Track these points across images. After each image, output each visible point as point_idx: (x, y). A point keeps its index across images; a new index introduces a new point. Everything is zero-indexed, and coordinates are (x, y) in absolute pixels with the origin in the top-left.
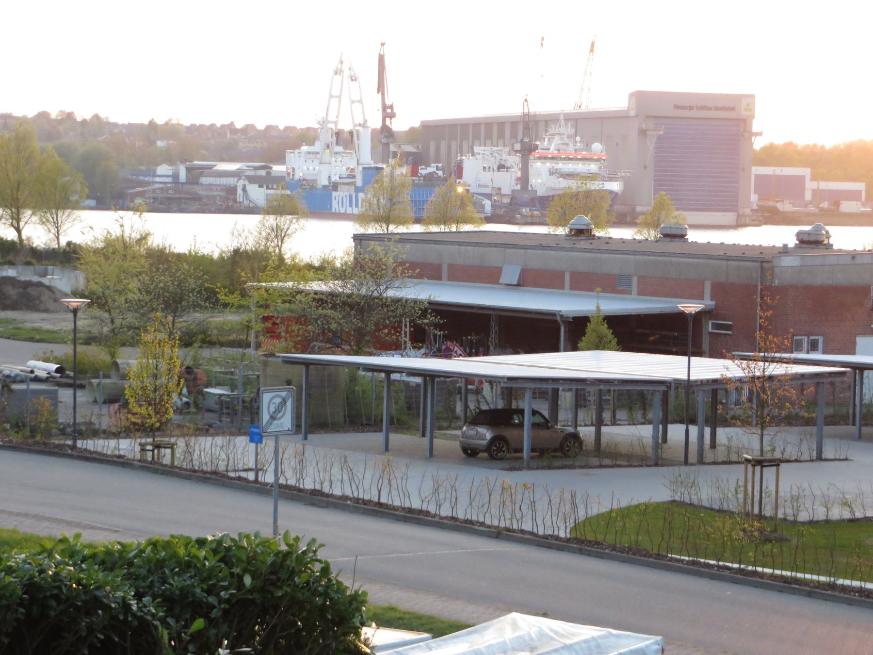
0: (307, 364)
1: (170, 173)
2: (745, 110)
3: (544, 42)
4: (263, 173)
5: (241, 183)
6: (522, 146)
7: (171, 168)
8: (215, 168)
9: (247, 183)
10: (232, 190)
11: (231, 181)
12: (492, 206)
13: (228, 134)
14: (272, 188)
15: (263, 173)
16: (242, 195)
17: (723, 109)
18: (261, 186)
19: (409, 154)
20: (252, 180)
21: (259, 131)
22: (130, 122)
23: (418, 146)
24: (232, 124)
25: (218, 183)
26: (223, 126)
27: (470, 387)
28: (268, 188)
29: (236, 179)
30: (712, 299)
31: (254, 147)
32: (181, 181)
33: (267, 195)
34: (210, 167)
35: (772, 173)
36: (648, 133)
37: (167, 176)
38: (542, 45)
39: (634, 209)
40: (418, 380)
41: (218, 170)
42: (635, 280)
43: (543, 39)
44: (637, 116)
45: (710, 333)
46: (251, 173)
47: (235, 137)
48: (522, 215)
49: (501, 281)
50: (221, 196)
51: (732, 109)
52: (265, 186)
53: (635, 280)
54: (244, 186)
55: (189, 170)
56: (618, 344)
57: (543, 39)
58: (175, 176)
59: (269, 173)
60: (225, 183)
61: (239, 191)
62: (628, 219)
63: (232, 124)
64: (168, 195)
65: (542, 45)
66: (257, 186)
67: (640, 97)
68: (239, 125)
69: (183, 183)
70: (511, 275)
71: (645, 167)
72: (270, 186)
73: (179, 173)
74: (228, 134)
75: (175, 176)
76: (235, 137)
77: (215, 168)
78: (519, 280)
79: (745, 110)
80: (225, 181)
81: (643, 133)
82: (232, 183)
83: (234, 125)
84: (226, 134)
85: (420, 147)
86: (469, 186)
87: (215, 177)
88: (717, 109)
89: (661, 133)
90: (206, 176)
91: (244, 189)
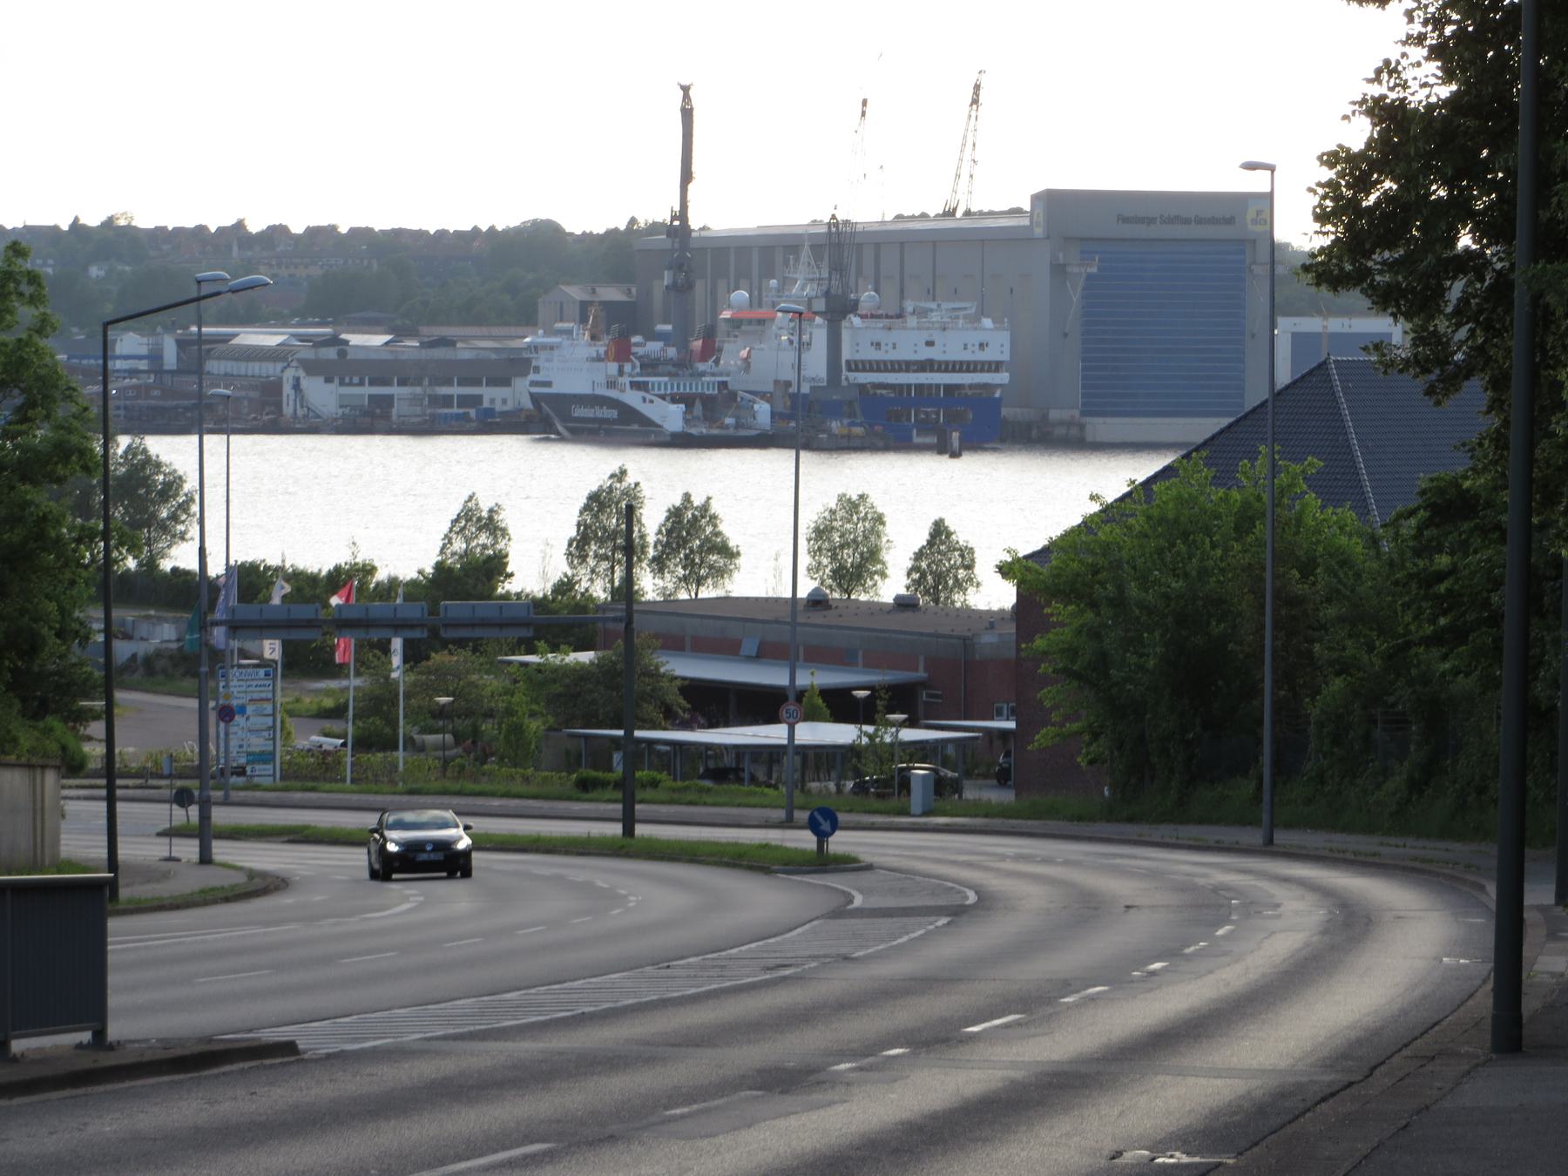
0: (586, 737)
1: (144, 351)
2: (1254, 222)
3: (868, 110)
4: (331, 353)
5: (289, 374)
6: (827, 304)
7: (145, 340)
8: (235, 341)
9: (301, 373)
10: (272, 389)
11: (270, 369)
12: (773, 414)
13: (235, 249)
14: (351, 384)
15: (331, 353)
16: (292, 397)
17: (1213, 221)
18: (329, 380)
19: (608, 306)
20: (312, 368)
21: (297, 237)
22: (30, 223)
23: (629, 290)
24: (240, 225)
25: (243, 372)
26: (221, 230)
27: (709, 752)
28: (342, 383)
29: (279, 366)
30: (925, 671)
31: (291, 276)
32: (166, 367)
33: (341, 396)
34: (226, 339)
35: (1320, 330)
36: (1069, 269)
37: (140, 358)
38: (863, 114)
39: (1045, 417)
40: (668, 748)
41: (240, 346)
42: (860, 653)
43: (865, 103)
44: (1048, 238)
45: (926, 703)
46: (308, 354)
47: (249, 253)
48: (831, 435)
49: (741, 653)
50: (251, 400)
51: (1230, 221)
52: (337, 380)
53: (860, 653)
54: (297, 380)
55: (182, 344)
56: (831, 715)
57: (865, 103)
58: (155, 357)
59: (342, 354)
60: (257, 372)
61: (287, 389)
62: (1034, 433)
63: (240, 225)
64: (153, 402)
65: (863, 114)
66: (321, 379)
67: (1053, 203)
68: (255, 226)
69: (171, 372)
70: (749, 647)
71: (1066, 335)
72: (347, 380)
73: (162, 350)
74: (235, 249)
75: (155, 357)
76: (249, 253)
77: (235, 341)
78: (758, 652)
79: (1254, 222)
80: (255, 368)
81: (1058, 270)
82: (271, 371)
83: (244, 227)
84: (229, 248)
85: (634, 290)
86: (728, 375)
87: (236, 359)
88: (1200, 221)
89: (1094, 270)
90: (219, 358)
91: (297, 386)
